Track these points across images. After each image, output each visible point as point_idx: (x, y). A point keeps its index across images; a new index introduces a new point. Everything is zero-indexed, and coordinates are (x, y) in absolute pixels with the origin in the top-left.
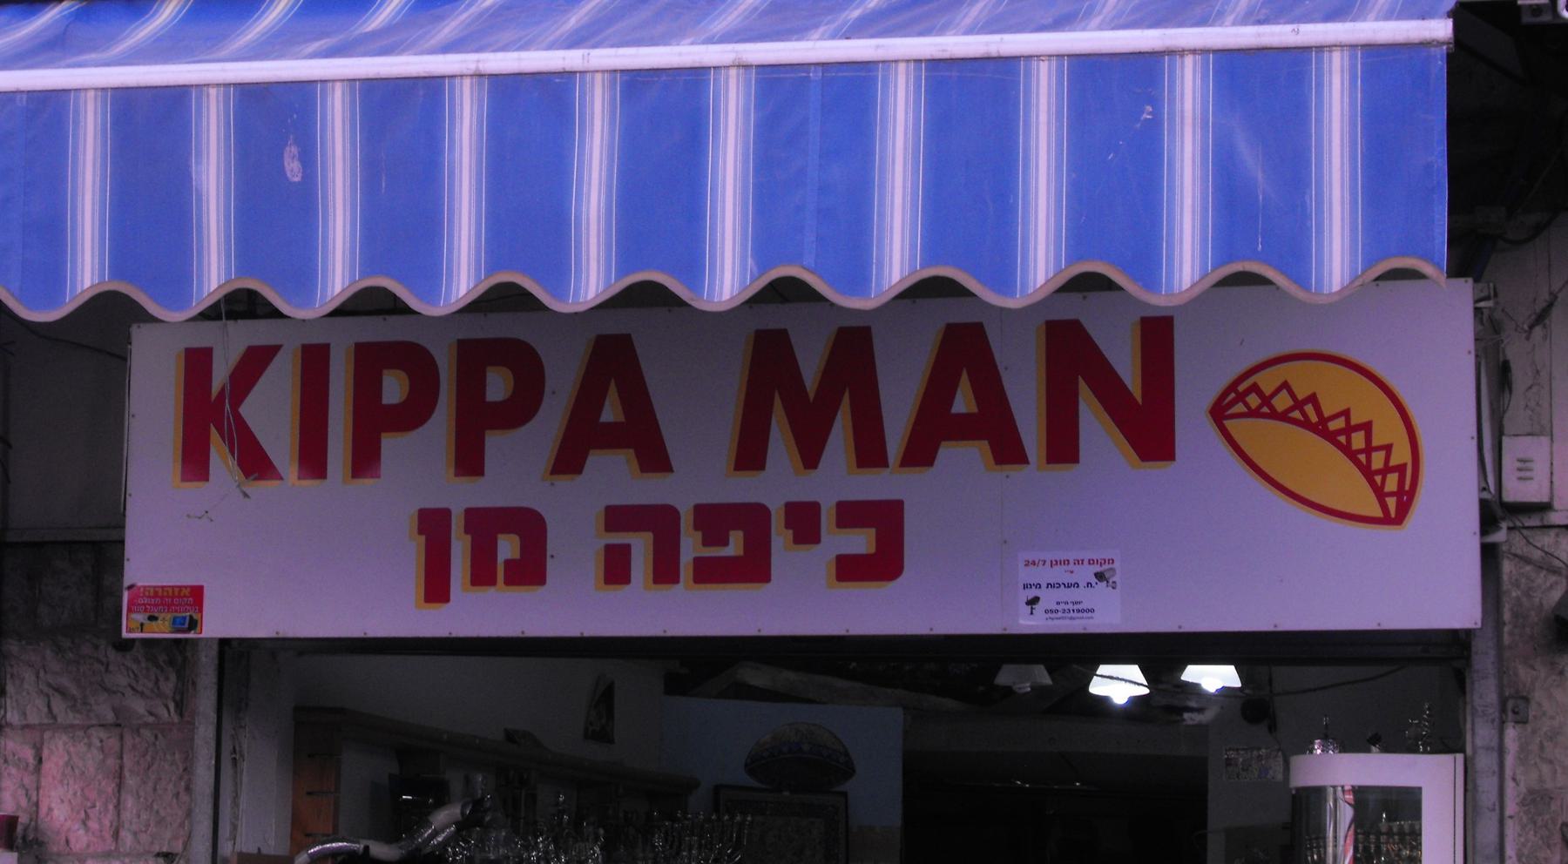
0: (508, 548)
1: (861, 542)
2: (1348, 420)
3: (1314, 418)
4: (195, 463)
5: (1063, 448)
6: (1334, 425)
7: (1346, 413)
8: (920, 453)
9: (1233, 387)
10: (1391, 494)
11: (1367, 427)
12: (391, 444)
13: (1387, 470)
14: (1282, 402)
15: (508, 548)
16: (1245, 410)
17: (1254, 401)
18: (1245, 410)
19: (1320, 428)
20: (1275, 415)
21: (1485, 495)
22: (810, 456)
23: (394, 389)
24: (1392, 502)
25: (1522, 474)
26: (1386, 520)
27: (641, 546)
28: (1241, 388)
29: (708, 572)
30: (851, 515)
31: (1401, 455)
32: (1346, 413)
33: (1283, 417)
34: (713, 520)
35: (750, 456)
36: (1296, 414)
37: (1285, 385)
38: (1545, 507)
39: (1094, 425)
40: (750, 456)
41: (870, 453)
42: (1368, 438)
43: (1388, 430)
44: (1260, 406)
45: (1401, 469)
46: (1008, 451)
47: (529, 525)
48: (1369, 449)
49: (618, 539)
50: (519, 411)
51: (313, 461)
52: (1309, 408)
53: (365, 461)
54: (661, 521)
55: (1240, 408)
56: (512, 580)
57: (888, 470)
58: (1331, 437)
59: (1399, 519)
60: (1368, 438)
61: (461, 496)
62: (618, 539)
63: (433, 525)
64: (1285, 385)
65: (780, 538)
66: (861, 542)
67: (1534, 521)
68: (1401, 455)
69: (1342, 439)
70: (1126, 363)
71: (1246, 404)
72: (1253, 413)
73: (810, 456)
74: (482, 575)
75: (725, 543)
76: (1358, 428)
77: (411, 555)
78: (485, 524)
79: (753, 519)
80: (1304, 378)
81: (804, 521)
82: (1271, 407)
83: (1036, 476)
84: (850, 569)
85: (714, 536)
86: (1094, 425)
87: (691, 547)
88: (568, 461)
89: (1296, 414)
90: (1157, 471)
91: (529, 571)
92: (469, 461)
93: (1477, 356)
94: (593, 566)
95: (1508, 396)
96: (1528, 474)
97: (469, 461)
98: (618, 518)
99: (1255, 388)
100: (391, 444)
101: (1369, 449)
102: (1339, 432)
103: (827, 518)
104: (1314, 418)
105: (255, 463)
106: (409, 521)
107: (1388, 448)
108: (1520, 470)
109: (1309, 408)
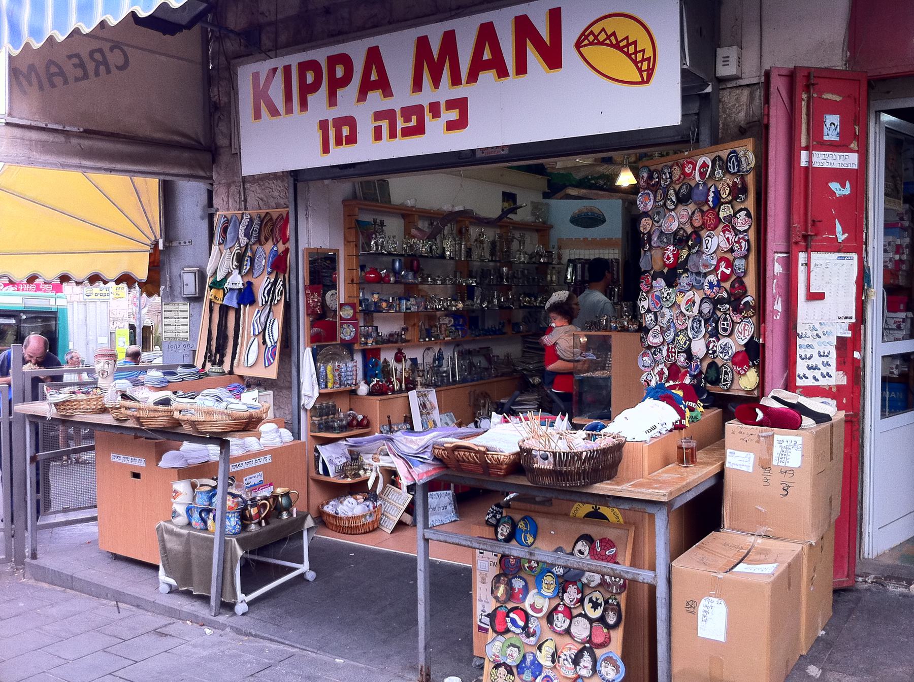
0: (346, 131)
1: (454, 115)
2: (628, 41)
3: (614, 42)
4: (257, 116)
5: (521, 69)
6: (621, 44)
7: (627, 38)
8: (473, 77)
9: (583, 34)
10: (644, 71)
11: (635, 43)
12: (310, 98)
13: (643, 60)
14: (602, 37)
15: (346, 131)
16: (588, 42)
17: (591, 38)
18: (588, 42)
19: (617, 46)
20: (600, 43)
21: (685, 67)
22: (436, 82)
23: (310, 78)
24: (645, 74)
25: (725, 63)
26: (643, 82)
27: (385, 125)
28: (586, 34)
29: (407, 132)
30: (451, 104)
31: (649, 53)
32: (627, 38)
33: (602, 43)
34: (407, 112)
35: (417, 85)
36: (608, 42)
37: (603, 30)
38: (736, 78)
39: (533, 57)
40: (417, 85)
41: (456, 80)
42: (616, 38)
43: (644, 43)
44: (594, 40)
45: (649, 59)
46: (503, 73)
47: (351, 122)
48: (636, 52)
49: (378, 123)
50: (346, 81)
51: (289, 111)
52: (613, 38)
53: (304, 105)
54: (389, 115)
55: (586, 42)
56: (347, 143)
57: (462, 86)
58: (621, 49)
59: (648, 82)
60: (616, 38)
61: (331, 114)
62: (378, 123)
63: (323, 125)
64: (603, 30)
65: (428, 116)
66: (454, 115)
67: (733, 84)
68: (649, 53)
69: (625, 50)
70: (544, 32)
71: (589, 40)
72: (591, 44)
73: (436, 82)
74: (339, 143)
75: (411, 121)
76: (611, 35)
77: (318, 135)
78: (340, 123)
79: (418, 110)
80: (610, 25)
81: (435, 109)
82: (598, 40)
83: (513, 79)
84: (451, 126)
85: (408, 120)
86: (533, 57)
87: (400, 124)
88: (362, 95)
89: (608, 42)
90: (556, 73)
91: (352, 139)
92: (332, 100)
93: (680, 4)
94: (371, 134)
95: (755, 29)
96: (727, 63)
97: (332, 100)
98: (378, 116)
99: (592, 33)
100: (310, 98)
101: (636, 52)
102: (624, 47)
103: (443, 107)
104: (614, 42)
105: (274, 112)
106: (316, 126)
107: (643, 51)
108: (723, 61)
109: (613, 38)
